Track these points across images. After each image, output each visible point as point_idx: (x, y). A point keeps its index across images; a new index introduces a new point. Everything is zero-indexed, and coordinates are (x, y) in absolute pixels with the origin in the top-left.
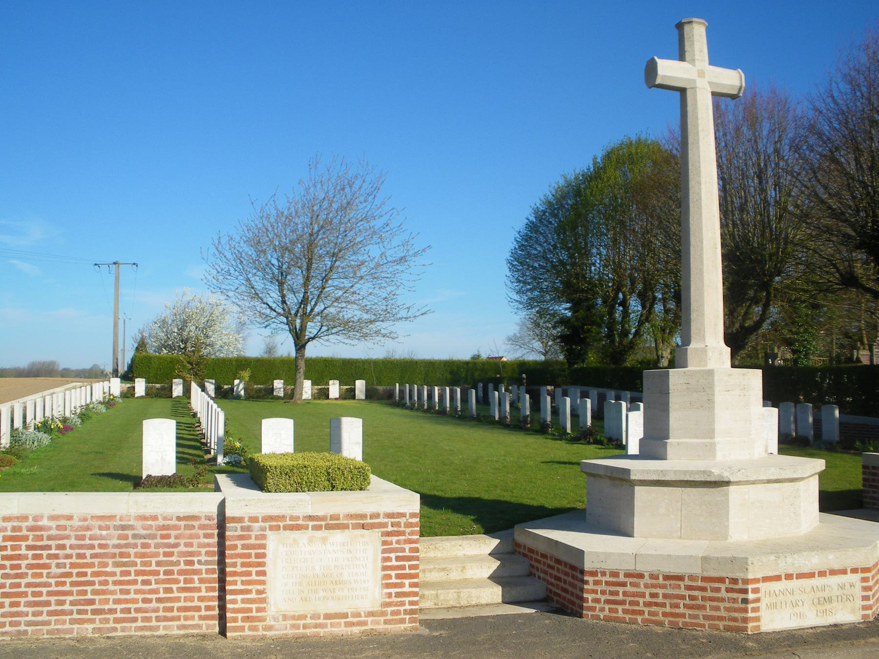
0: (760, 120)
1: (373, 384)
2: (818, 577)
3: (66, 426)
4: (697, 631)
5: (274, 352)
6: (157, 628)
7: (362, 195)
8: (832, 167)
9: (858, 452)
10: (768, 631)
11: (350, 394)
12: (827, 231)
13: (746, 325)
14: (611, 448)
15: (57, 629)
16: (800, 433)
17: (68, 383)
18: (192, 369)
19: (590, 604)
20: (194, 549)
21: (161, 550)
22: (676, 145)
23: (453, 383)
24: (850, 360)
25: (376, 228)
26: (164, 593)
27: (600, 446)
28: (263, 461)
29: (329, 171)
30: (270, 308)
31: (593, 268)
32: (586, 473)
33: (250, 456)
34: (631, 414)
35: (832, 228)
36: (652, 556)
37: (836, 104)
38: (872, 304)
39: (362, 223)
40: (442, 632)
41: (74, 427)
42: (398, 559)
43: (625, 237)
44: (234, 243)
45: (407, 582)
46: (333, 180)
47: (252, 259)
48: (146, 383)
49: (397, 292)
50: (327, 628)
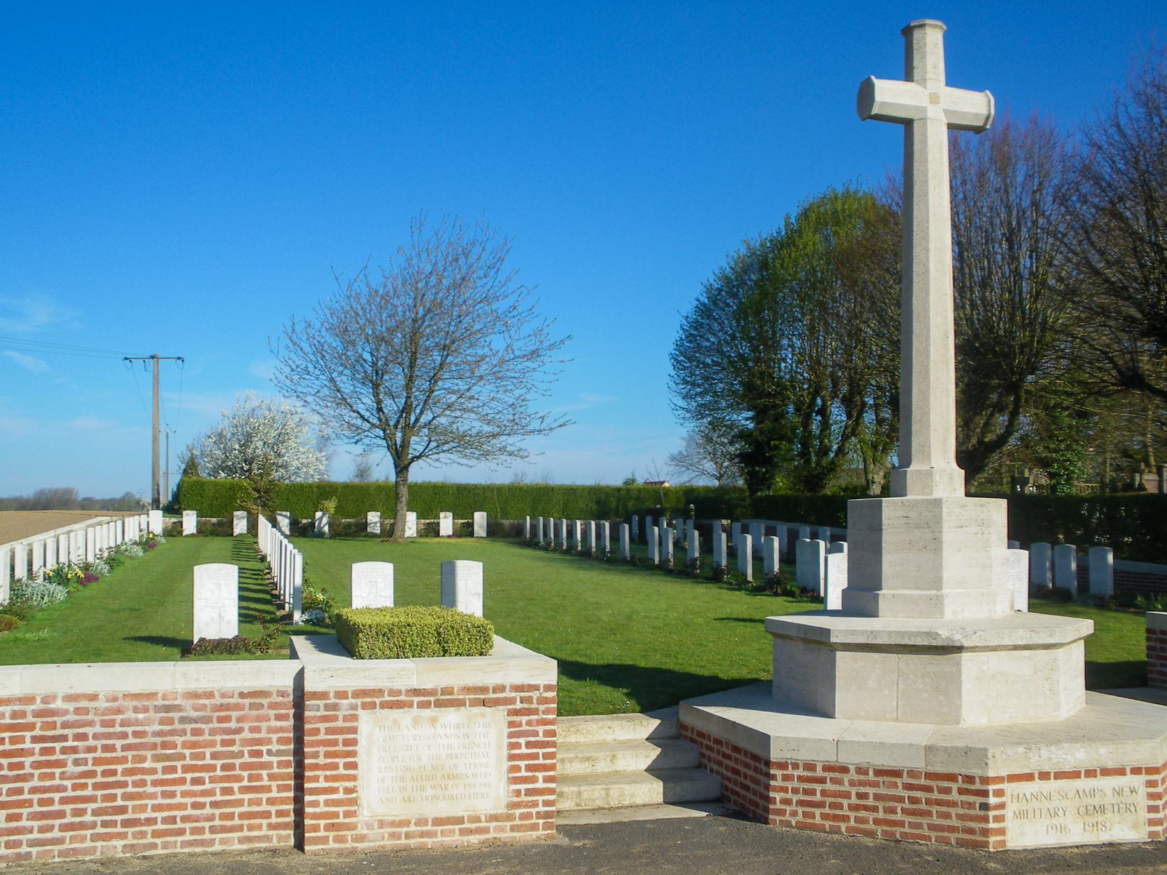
0: (1014, 161)
1: (496, 517)
2: (1085, 777)
3: (89, 576)
4: (920, 845)
5: (367, 475)
6: (212, 842)
7: (481, 268)
8: (1112, 225)
9: (1140, 611)
10: (1016, 849)
11: (466, 530)
12: (1102, 313)
13: (987, 440)
14: (805, 602)
15: (73, 849)
16: (1059, 584)
17: (90, 517)
18: (259, 498)
19: (778, 806)
20: (263, 735)
21: (218, 738)
22: (897, 199)
23: (600, 515)
24: (1130, 486)
25: (500, 312)
26: (222, 794)
27: (790, 599)
28: (354, 618)
29: (437, 235)
30: (362, 417)
31: (783, 365)
32: (772, 634)
33: (336, 611)
34: (830, 556)
35: (1109, 309)
36: (859, 743)
37: (1123, 135)
38: (1163, 411)
39: (482, 305)
40: (586, 842)
41: (100, 576)
43: (826, 324)
44: (313, 332)
45: (540, 775)
46: (443, 248)
47: (337, 353)
48: (197, 517)
49: (528, 397)
50: (436, 837)
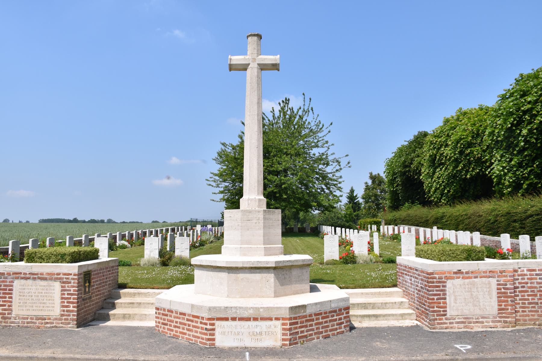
42: (68, 294)
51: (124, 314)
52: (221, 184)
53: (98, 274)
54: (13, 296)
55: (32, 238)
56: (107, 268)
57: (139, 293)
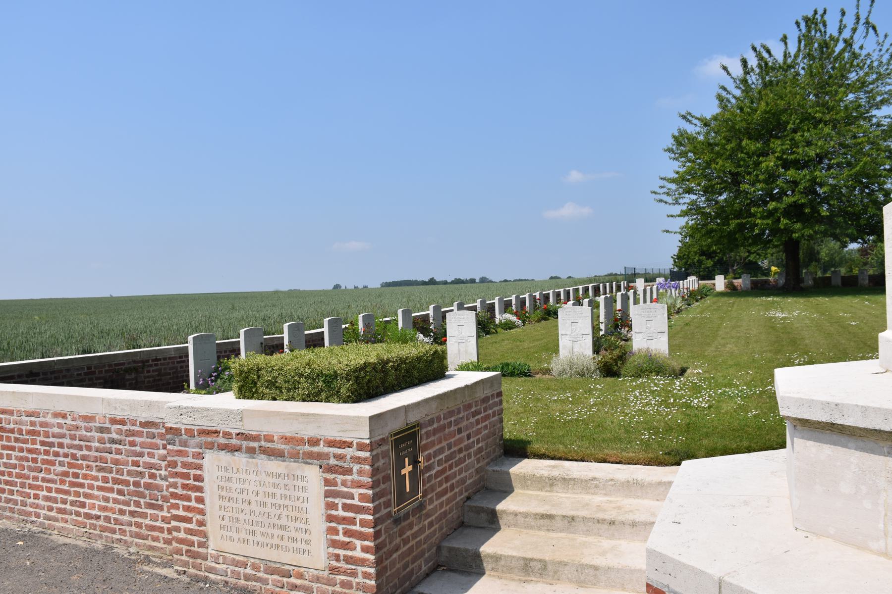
42: (346, 507)
51: (525, 559)
52: (683, 197)
53: (442, 428)
54: (206, 495)
55: (328, 317)
56: (469, 406)
57: (564, 479)
